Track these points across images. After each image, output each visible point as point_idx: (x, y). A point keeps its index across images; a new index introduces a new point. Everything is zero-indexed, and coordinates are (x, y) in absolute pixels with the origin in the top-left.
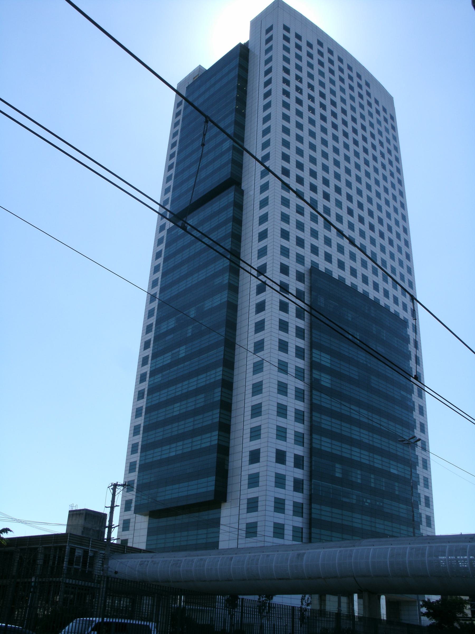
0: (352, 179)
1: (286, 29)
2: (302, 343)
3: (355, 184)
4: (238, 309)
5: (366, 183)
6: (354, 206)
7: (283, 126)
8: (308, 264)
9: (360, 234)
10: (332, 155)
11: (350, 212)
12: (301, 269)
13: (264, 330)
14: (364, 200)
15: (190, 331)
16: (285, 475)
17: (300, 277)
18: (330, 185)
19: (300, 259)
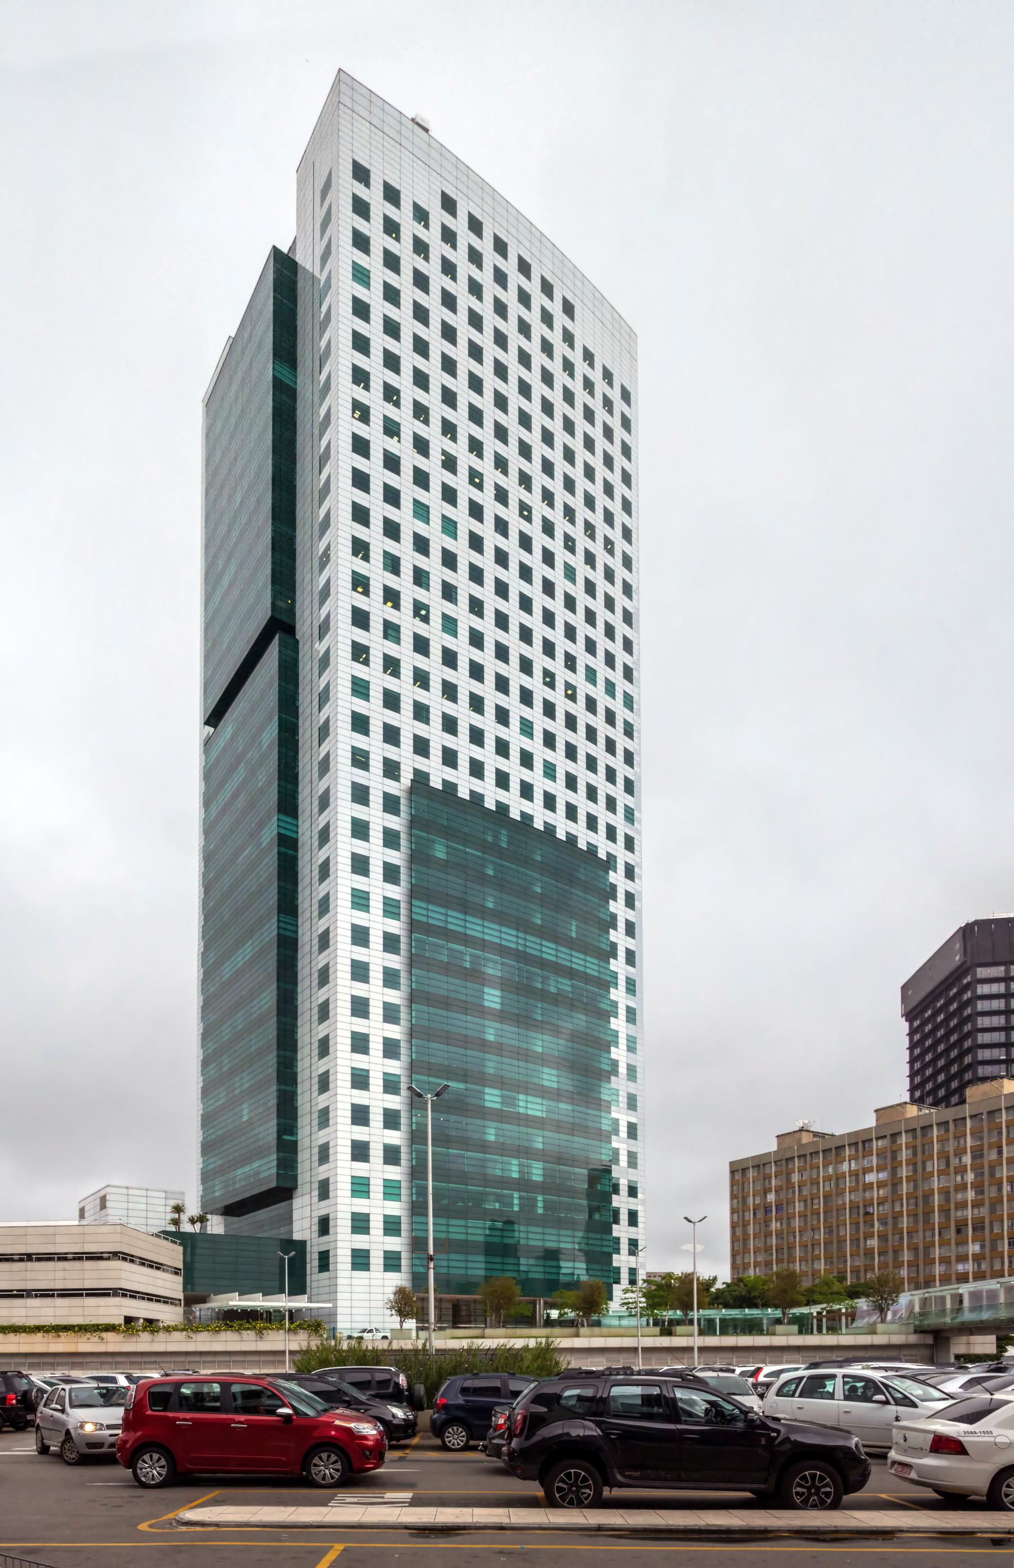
0: (533, 318)
1: (361, 174)
2: (396, 962)
3: (538, 329)
4: (300, 778)
5: (593, 454)
6: (534, 378)
7: (354, 469)
8: (407, 776)
9: (565, 574)
10: (465, 269)
11: (525, 420)
12: (394, 788)
13: (328, 1126)
14: (577, 386)
15: (245, 1112)
16: (368, 964)
17: (391, 804)
18: (458, 340)
19: (391, 769)
